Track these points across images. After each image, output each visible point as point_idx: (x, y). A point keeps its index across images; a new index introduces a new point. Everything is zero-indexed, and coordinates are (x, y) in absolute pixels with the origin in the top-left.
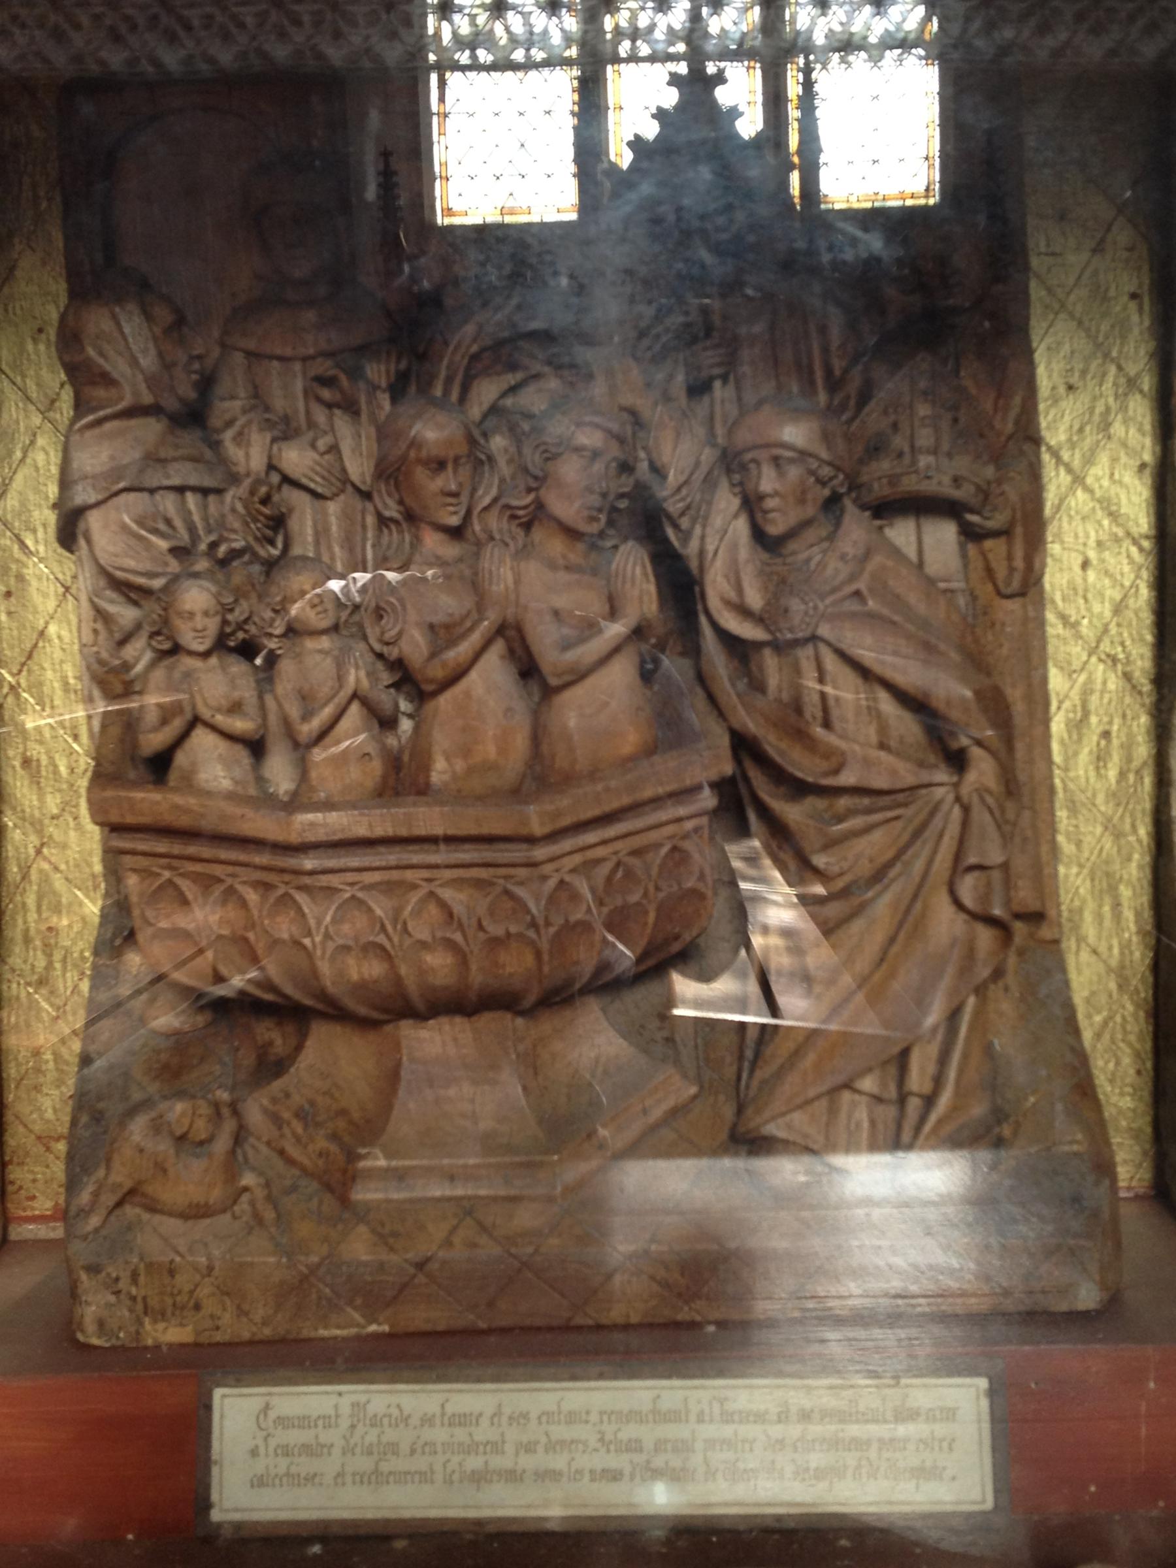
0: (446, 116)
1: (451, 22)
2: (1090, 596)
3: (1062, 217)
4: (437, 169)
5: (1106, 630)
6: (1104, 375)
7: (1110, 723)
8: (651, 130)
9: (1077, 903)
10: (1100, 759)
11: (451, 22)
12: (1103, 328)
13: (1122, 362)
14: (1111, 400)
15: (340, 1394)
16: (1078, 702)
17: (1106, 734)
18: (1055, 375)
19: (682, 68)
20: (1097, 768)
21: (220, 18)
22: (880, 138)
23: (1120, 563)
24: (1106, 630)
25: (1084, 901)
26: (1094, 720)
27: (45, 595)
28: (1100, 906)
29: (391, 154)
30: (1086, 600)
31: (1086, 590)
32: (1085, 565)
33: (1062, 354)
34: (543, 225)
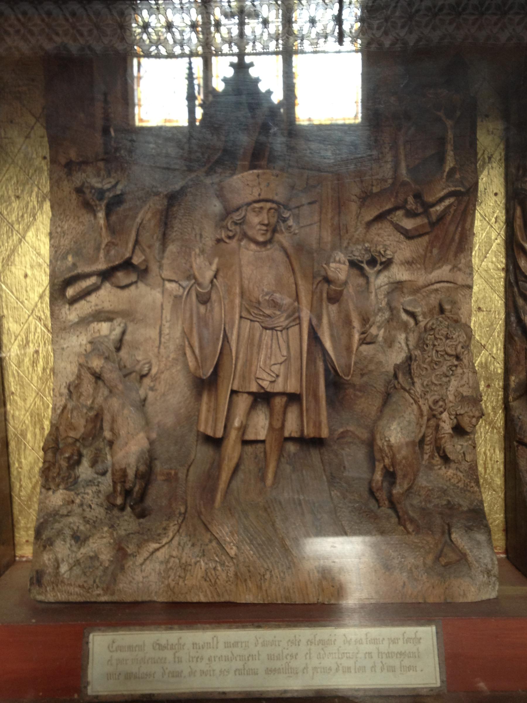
2: (28, 289)
3: (12, 122)
5: (36, 305)
6: (32, 192)
7: (39, 346)
9: (24, 427)
10: (34, 363)
12: (31, 171)
13: (40, 187)
14: (35, 203)
16: (24, 337)
17: (37, 352)
18: (10, 191)
19: (235, 60)
20: (33, 366)
21: (22, 31)
22: (330, 89)
23: (41, 275)
24: (36, 305)
25: (27, 427)
26: (31, 345)
28: (35, 429)
30: (27, 291)
31: (26, 287)
32: (26, 276)
33: (13, 182)
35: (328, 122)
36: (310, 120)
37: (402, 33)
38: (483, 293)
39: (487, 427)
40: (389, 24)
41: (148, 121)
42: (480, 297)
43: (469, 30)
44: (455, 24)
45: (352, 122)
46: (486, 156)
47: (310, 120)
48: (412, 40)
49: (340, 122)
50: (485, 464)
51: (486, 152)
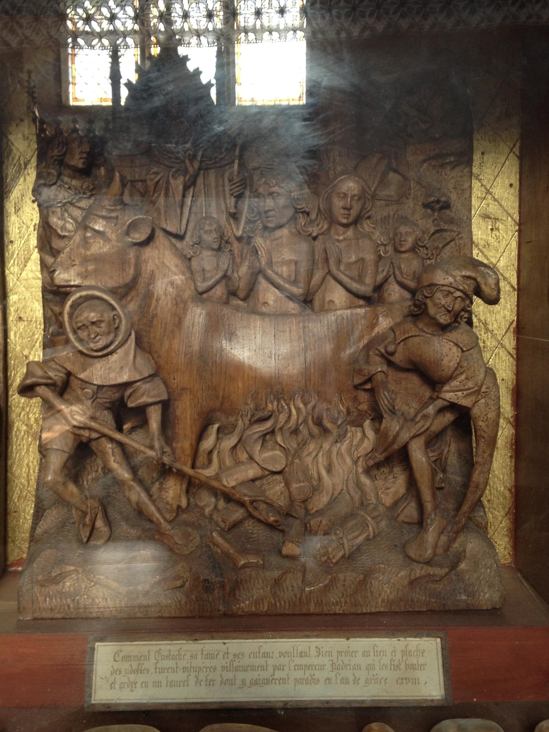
0: (75, 55)
1: (160, 11)
4: (71, 79)
8: (191, 66)
11: (160, 11)
15: (224, 643)
22: (275, 73)
27: (224, 264)
29: (32, 72)
34: (93, 107)
35: (272, 103)
36: (252, 100)
37: (371, 21)
38: (24, 303)
39: (30, 440)
40: (381, 10)
41: (83, 100)
42: (21, 306)
43: (436, 19)
44: (399, 13)
45: (296, 103)
46: (22, 162)
47: (252, 100)
48: (380, 27)
49: (284, 103)
50: (28, 476)
51: (22, 158)
